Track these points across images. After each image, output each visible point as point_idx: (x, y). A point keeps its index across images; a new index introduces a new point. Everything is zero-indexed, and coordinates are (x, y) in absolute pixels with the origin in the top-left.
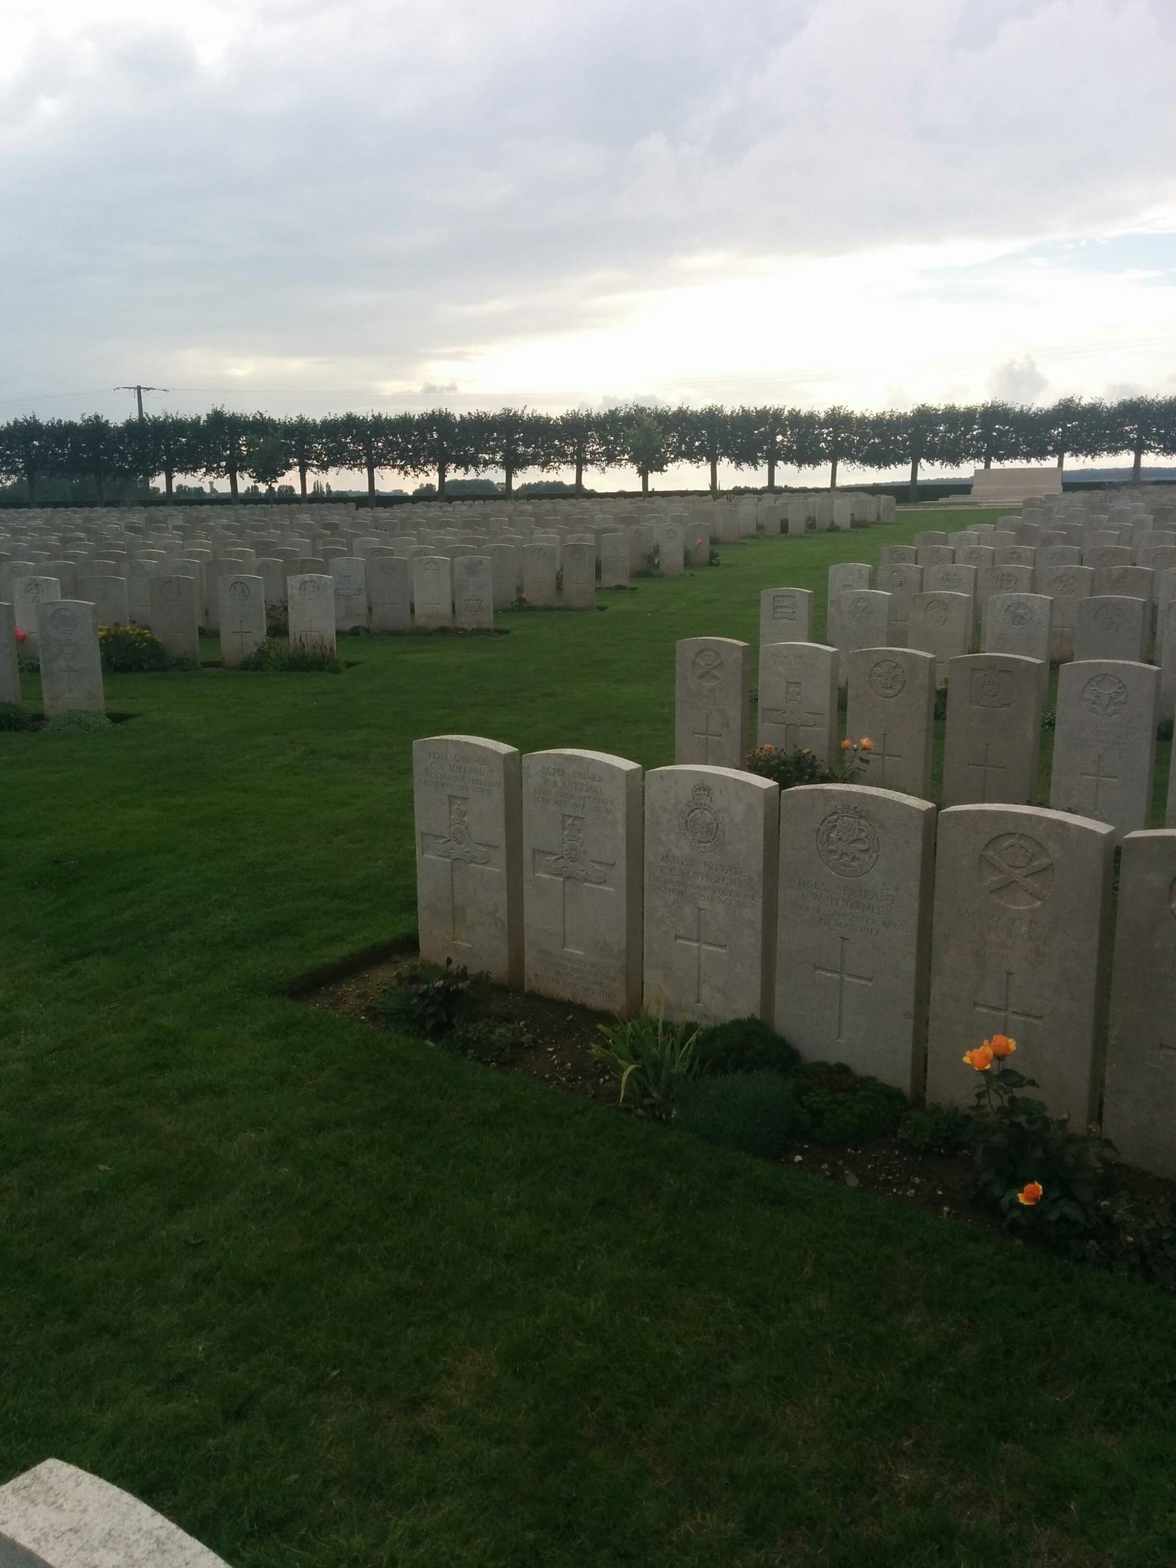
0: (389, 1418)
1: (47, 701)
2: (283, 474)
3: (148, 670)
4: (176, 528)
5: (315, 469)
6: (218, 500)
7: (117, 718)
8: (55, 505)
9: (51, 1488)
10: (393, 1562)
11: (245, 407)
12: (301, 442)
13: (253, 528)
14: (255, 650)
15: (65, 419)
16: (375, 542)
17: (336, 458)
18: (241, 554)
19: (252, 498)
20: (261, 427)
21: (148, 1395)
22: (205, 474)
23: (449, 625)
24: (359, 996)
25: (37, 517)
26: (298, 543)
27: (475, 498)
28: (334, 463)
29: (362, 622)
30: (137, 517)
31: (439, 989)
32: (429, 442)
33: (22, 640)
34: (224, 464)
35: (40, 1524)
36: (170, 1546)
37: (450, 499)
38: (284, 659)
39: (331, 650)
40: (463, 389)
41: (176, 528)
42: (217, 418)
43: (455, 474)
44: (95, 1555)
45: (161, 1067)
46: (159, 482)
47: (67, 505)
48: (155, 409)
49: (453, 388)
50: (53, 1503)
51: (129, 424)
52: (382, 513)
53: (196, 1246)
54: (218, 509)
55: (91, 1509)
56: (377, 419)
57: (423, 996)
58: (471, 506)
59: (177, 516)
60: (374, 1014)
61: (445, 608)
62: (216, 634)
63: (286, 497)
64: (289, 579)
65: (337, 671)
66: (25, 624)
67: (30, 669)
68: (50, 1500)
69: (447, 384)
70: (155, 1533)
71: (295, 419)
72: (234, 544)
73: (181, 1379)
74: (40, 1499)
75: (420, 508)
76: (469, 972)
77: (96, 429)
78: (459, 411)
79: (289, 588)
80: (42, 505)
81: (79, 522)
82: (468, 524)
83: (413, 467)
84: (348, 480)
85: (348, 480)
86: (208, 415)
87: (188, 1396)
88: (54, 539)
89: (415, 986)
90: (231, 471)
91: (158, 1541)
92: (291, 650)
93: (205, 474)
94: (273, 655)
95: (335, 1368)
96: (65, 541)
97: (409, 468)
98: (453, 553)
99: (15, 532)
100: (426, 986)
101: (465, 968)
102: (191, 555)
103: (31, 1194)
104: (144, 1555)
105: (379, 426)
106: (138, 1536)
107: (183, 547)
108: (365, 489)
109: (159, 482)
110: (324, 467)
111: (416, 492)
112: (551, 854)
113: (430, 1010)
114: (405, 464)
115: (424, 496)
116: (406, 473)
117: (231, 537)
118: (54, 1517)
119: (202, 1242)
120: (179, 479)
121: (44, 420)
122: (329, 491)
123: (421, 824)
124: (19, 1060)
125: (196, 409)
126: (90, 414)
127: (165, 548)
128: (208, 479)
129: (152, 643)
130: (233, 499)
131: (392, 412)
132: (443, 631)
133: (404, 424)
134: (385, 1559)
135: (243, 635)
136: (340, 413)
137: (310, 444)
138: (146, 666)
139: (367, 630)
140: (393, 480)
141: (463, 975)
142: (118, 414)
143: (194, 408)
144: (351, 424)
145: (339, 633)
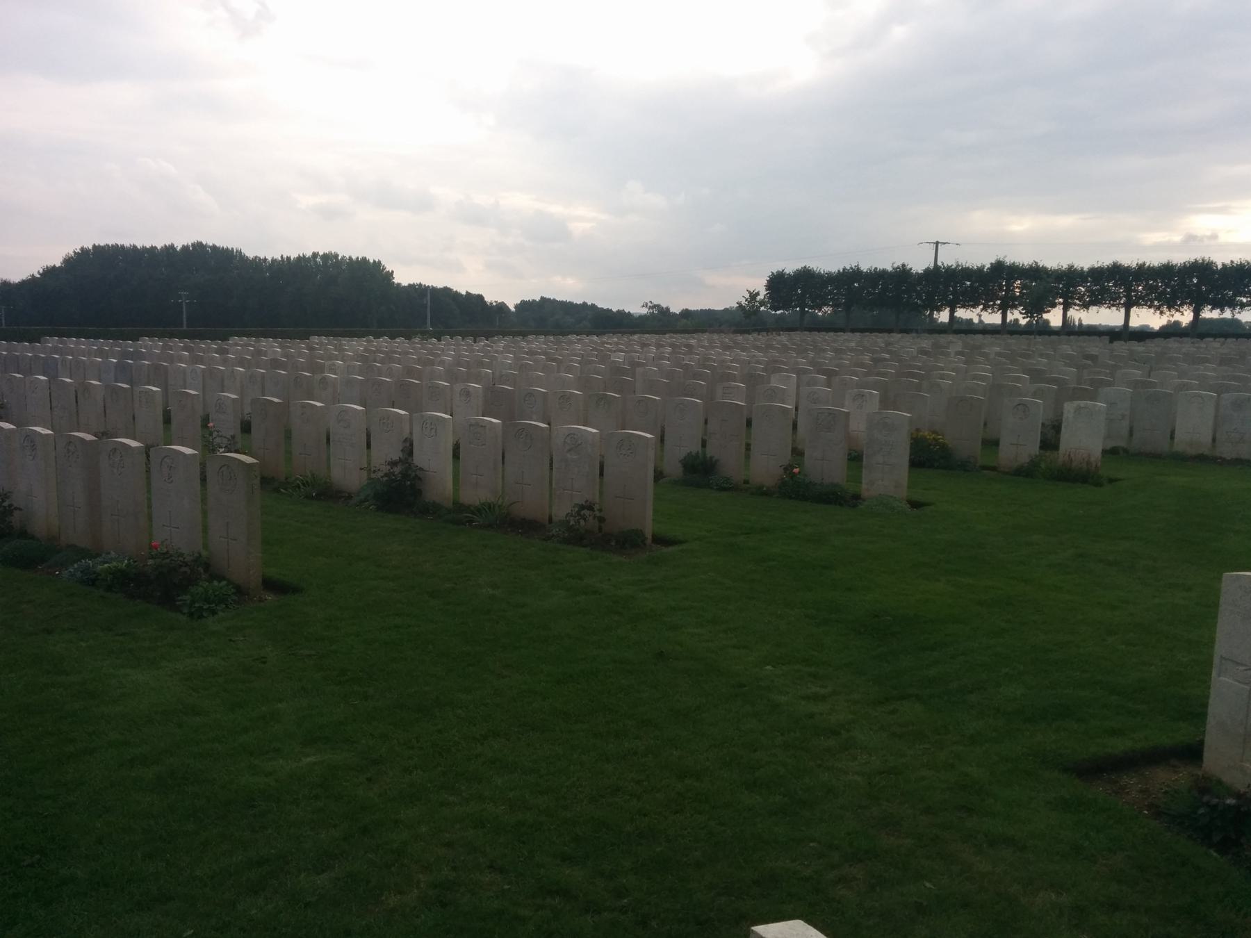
1: (864, 486)
6: (1113, 335)
7: (915, 505)
8: (862, 331)
11: (1023, 258)
12: (1067, 286)
15: (880, 267)
16: (1137, 374)
17: (1096, 300)
18: (1018, 379)
20: (1035, 273)
23: (1207, 452)
24: (1141, 791)
25: (851, 340)
26: (1069, 373)
27: (1226, 336)
29: (1122, 444)
30: (926, 342)
32: (1189, 286)
37: (1202, 336)
38: (1052, 470)
40: (1224, 238)
42: (999, 267)
43: (1209, 314)
46: (943, 316)
47: (871, 331)
48: (948, 259)
49: (1214, 237)
51: (927, 271)
52: (1138, 347)
56: (1141, 267)
57: (1215, 807)
59: (957, 343)
61: (1205, 435)
63: (1044, 330)
64: (1066, 405)
65: (1098, 484)
66: (858, 426)
67: (855, 458)
69: (1208, 234)
75: (1173, 343)
77: (902, 275)
78: (1221, 259)
80: (853, 331)
82: (1224, 361)
83: (1169, 308)
84: (1106, 316)
85: (1106, 316)
88: (866, 358)
90: (1004, 308)
94: (1043, 465)
96: (876, 361)
102: (975, 377)
105: (1143, 273)
110: (1086, 306)
111: (1163, 328)
112: (1242, 665)
115: (1171, 331)
116: (1162, 313)
120: (961, 313)
121: (864, 268)
122: (1081, 324)
125: (981, 259)
126: (898, 263)
129: (944, 447)
131: (1155, 259)
132: (1201, 458)
133: (1167, 271)
135: (1019, 445)
136: (1105, 261)
139: (1126, 451)
140: (1147, 318)
142: (919, 263)
144: (1117, 273)
145: (1104, 452)
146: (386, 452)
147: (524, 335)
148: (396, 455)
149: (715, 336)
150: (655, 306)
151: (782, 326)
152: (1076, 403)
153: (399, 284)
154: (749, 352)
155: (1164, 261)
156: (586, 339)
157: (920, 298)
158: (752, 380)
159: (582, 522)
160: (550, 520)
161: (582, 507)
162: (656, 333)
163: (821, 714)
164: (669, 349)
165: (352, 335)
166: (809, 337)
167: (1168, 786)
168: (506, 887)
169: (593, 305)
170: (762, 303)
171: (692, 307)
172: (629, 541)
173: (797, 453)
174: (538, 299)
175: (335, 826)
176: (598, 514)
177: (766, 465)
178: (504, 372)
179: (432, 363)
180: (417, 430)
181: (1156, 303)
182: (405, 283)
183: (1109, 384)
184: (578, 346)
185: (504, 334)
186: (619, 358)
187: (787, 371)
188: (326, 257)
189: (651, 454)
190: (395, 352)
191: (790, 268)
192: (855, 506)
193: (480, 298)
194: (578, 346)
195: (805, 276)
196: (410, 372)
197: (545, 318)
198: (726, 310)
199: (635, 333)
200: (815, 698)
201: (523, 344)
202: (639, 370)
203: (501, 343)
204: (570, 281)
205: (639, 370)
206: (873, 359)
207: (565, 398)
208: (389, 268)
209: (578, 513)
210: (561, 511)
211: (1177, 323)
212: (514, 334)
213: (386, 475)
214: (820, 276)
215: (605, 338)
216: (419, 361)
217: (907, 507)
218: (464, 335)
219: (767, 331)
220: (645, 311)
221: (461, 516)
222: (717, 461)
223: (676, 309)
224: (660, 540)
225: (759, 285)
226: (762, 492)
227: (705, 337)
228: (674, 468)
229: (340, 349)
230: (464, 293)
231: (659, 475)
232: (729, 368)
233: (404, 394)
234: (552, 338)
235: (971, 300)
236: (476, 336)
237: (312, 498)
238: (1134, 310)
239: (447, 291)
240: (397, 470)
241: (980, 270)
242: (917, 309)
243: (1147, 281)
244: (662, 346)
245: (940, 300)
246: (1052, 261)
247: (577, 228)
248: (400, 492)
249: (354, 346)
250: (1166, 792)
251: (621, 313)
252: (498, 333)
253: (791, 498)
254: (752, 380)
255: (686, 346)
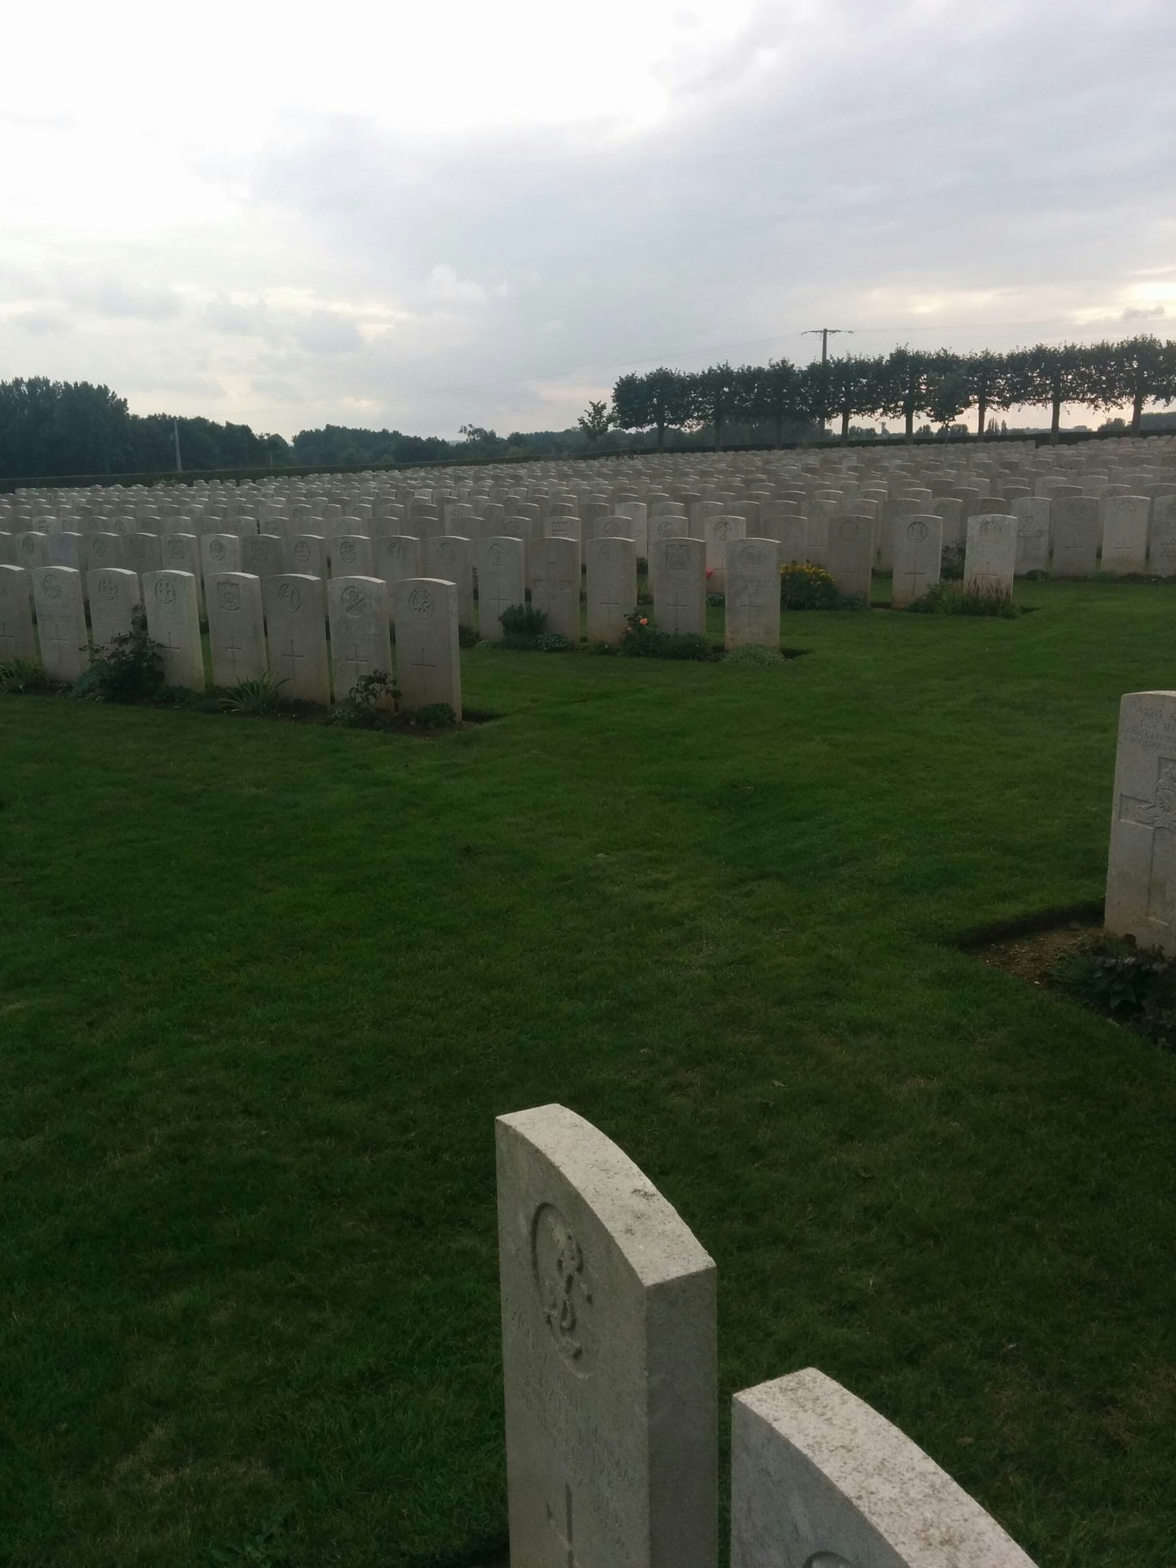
0: (1070, 1410)
1: (728, 635)
2: (962, 412)
3: (819, 608)
4: (849, 469)
5: (995, 406)
6: (1040, 438)
7: (790, 654)
8: (736, 449)
9: (817, 1399)
10: (1075, 1561)
11: (928, 345)
12: (983, 379)
13: (929, 468)
14: (927, 592)
15: (755, 365)
16: (1061, 480)
17: (1019, 393)
19: (925, 438)
20: (945, 364)
21: (821, 1314)
22: (881, 415)
23: (1140, 570)
24: (1033, 960)
25: (721, 461)
26: (977, 483)
28: (1017, 399)
29: (1040, 566)
30: (813, 458)
31: (1130, 967)
33: (709, 576)
34: (902, 403)
35: (812, 1432)
36: (944, 1496)
37: (1144, 434)
38: (953, 602)
39: (1007, 594)
41: (849, 469)
42: (900, 358)
43: (1153, 407)
44: (870, 1480)
45: (830, 995)
46: (835, 426)
47: (746, 448)
48: (839, 351)
49: (1159, 311)
50: (823, 1414)
51: (813, 367)
52: (1067, 451)
53: (865, 1180)
54: (892, 449)
55: (861, 1432)
57: (1110, 970)
58: (1170, 440)
59: (851, 457)
60: (1050, 982)
62: (889, 575)
63: (960, 436)
64: (970, 520)
65: (1010, 616)
66: (716, 561)
67: (716, 603)
68: (819, 1411)
69: (1152, 307)
70: (929, 1477)
71: (979, 354)
72: (910, 485)
73: (853, 1308)
74: (809, 1405)
75: (1109, 445)
76: (1165, 953)
77: (782, 374)
79: (969, 529)
81: (760, 464)
83: (1106, 401)
84: (1030, 416)
85: (1030, 416)
86: (891, 355)
87: (860, 1326)
88: (737, 481)
89: (1100, 959)
90: (908, 412)
91: (932, 1486)
92: (965, 591)
93: (881, 415)
94: (945, 597)
95: (1010, 1341)
96: (748, 483)
97: (1100, 402)
98: (1154, 492)
99: (703, 474)
100: (1114, 961)
101: (1161, 948)
103: (713, 1095)
104: (920, 1497)
105: (1072, 358)
106: (911, 1475)
107: (859, 487)
108: (1046, 425)
109: (835, 426)
110: (1005, 404)
111: (1102, 428)
113: (1117, 987)
114: (1096, 398)
115: (1113, 431)
116: (1096, 406)
117: (906, 477)
118: (825, 1429)
119: (872, 1178)
120: (859, 421)
121: (735, 367)
122: (1004, 429)
123: (1122, 784)
124: (701, 967)
125: (878, 350)
126: (777, 360)
127: (840, 489)
128: (885, 419)
130: (908, 439)
131: (1087, 342)
132: (1133, 578)
133: (1101, 355)
134: (1068, 1556)
135: (916, 575)
136: (1027, 345)
137: (993, 379)
138: (818, 604)
139: (1045, 575)
140: (1080, 415)
141: (1158, 956)
142: (803, 358)
143: (874, 347)
144: (1041, 359)
146: (112, 625)
147: (303, 473)
148: (125, 629)
149: (552, 464)
150: (477, 431)
151: (638, 447)
152: (981, 517)
153: (135, 417)
154: (598, 479)
155: (1098, 342)
156: (384, 475)
157: (807, 404)
158: (591, 512)
159: (372, 700)
160: (333, 700)
161: (370, 680)
162: (476, 463)
163: (662, 904)
164: (489, 482)
165: (69, 484)
166: (668, 459)
167: (1064, 951)
168: (263, 1132)
169: (396, 433)
170: (611, 419)
171: (525, 430)
172: (432, 720)
173: (645, 600)
174: (323, 428)
175: (45, 1082)
176: (391, 686)
177: (608, 617)
178: (270, 519)
179: (178, 513)
180: (149, 595)
181: (1089, 395)
182: (144, 415)
183: (1024, 493)
184: (373, 484)
185: (277, 474)
186: (425, 495)
187: (636, 499)
188: (34, 384)
189: (454, 606)
190: (129, 502)
191: (642, 371)
192: (717, 660)
193: (246, 430)
194: (372, 484)
195: (662, 382)
196: (147, 525)
197: (333, 452)
198: (567, 431)
199: (450, 465)
200: (657, 885)
201: (301, 485)
202: (449, 508)
203: (271, 485)
204: (365, 404)
205: (449, 508)
206: (744, 481)
207: (348, 545)
208: (120, 396)
209: (366, 687)
210: (345, 685)
211: (1119, 422)
212: (290, 474)
213: (113, 655)
214: (680, 380)
215: (409, 473)
216: (160, 511)
217: (779, 657)
218: (223, 478)
219: (618, 455)
220: (463, 438)
221: (216, 702)
222: (545, 616)
223: (503, 434)
224: (472, 716)
225: (606, 396)
226: (604, 651)
227: (537, 467)
228: (491, 627)
229: (54, 502)
230: (224, 424)
231: (468, 638)
232: (564, 500)
233: (136, 552)
234: (340, 476)
235: (866, 404)
236: (239, 478)
237: (20, 692)
238: (1064, 406)
239: (200, 423)
240: (128, 648)
241: (878, 363)
242: (802, 417)
243: (1077, 367)
244: (483, 478)
245: (830, 404)
246: (965, 348)
247: (371, 331)
248: (134, 676)
249: (74, 497)
250: (1061, 958)
251: (432, 442)
252: (268, 473)
253: (638, 655)
254: (591, 512)
255: (514, 477)
